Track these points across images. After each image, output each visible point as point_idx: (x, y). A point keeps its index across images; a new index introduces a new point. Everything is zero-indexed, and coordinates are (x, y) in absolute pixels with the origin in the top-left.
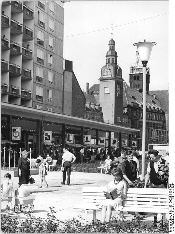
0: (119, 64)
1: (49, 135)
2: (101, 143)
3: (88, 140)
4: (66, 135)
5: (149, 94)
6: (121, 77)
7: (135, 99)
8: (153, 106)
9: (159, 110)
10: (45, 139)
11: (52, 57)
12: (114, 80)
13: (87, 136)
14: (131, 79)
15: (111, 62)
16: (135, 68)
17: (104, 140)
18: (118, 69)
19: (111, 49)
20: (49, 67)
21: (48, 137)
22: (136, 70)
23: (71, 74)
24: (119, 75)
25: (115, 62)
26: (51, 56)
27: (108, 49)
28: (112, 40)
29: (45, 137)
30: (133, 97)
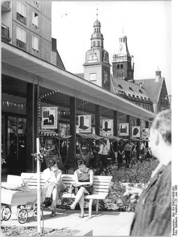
0: (106, 47)
1: (52, 116)
2: (122, 133)
3: (108, 127)
4: (77, 119)
5: (135, 83)
6: (108, 63)
7: (122, 88)
8: (140, 95)
9: (146, 100)
10: (44, 124)
11: (37, 17)
12: (101, 65)
13: (106, 120)
14: (115, 68)
15: (96, 45)
16: (118, 56)
17: (126, 128)
18: (104, 53)
19: (96, 31)
20: (34, 30)
21: (50, 119)
22: (121, 57)
23: (55, 54)
24: (106, 60)
25: (101, 46)
26: (36, 15)
27: (93, 31)
28: (97, 21)
29: (43, 119)
30: (120, 86)
